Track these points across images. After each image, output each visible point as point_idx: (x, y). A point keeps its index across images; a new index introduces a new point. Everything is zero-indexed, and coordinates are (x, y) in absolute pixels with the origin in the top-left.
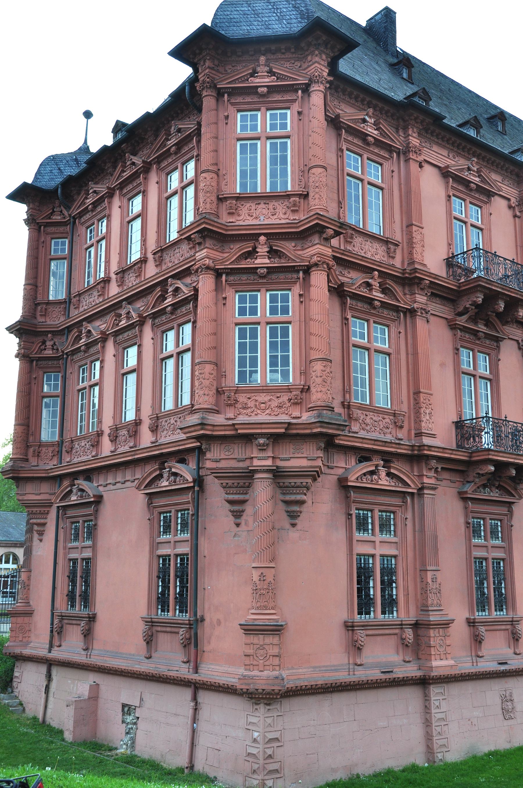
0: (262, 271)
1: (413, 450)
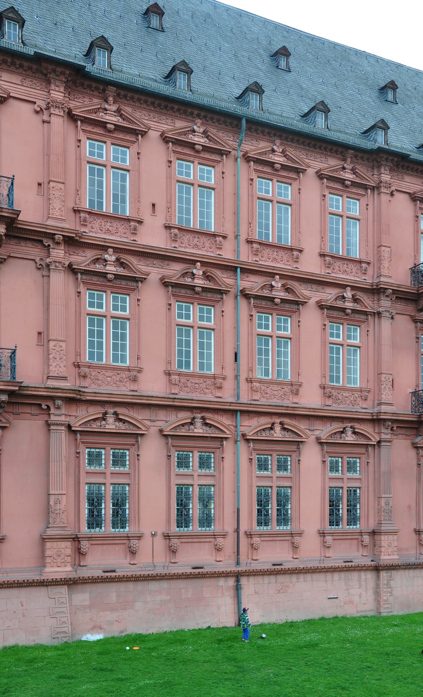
0: (199, 289)
1: (373, 416)
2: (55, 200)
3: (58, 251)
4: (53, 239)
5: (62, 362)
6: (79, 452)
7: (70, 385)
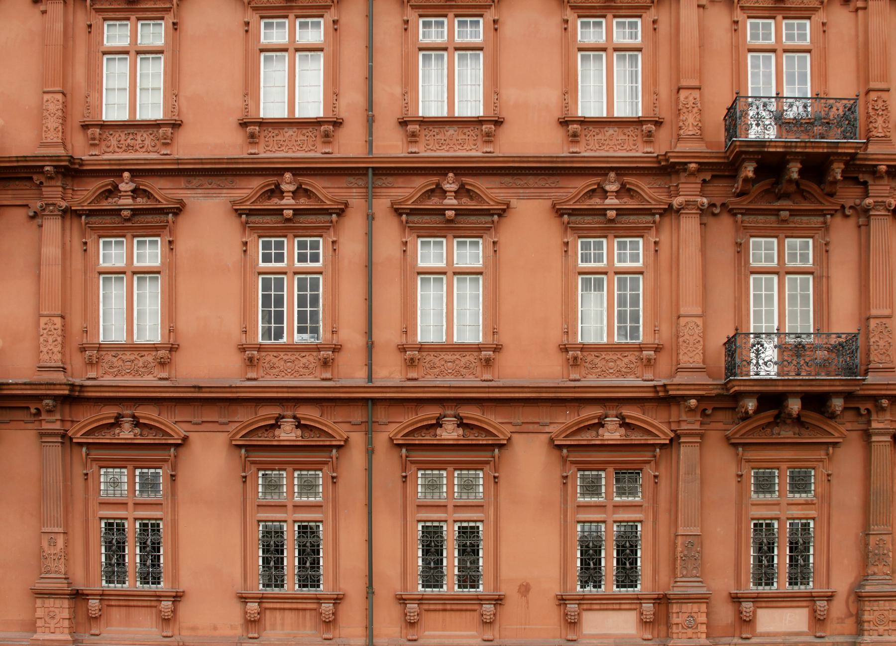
6: (567, 477)
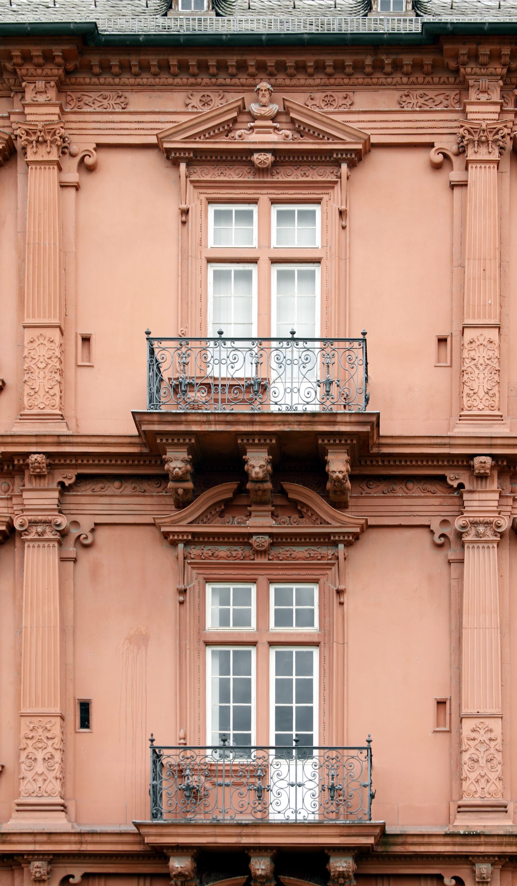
2: (477, 371)
3: (483, 496)
4: (470, 468)
5: (492, 767)
7: (511, 823)
